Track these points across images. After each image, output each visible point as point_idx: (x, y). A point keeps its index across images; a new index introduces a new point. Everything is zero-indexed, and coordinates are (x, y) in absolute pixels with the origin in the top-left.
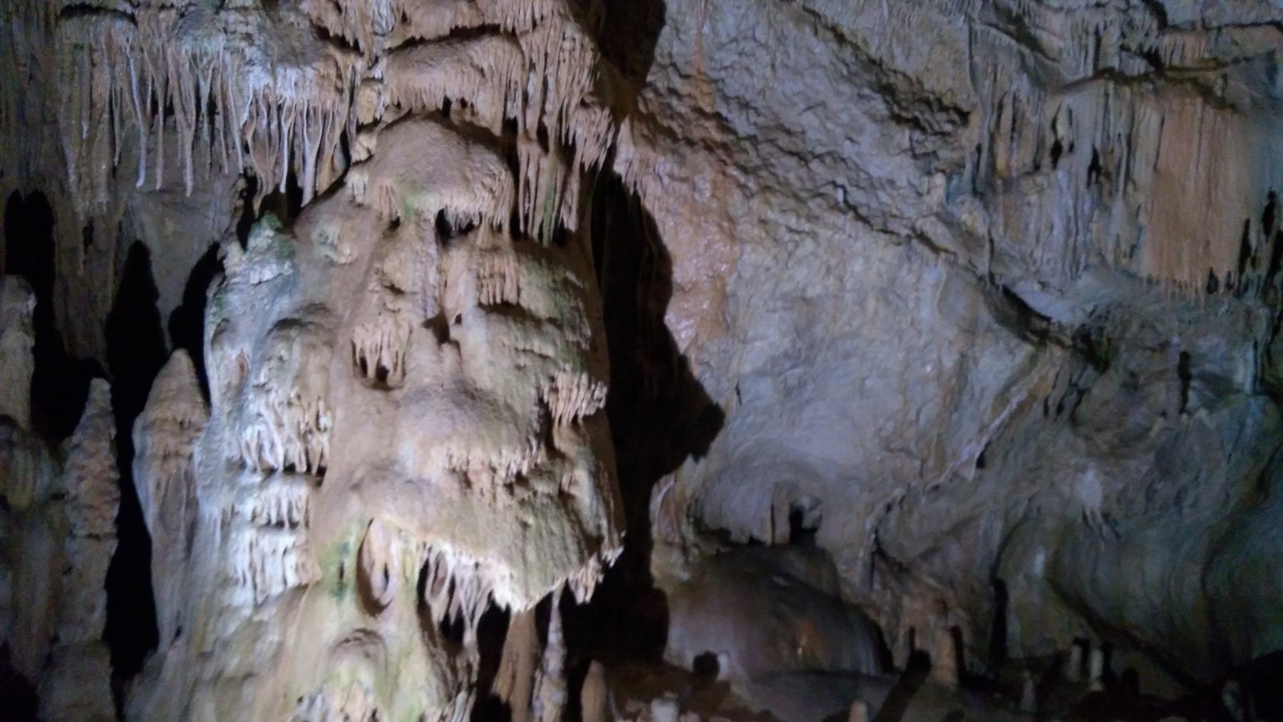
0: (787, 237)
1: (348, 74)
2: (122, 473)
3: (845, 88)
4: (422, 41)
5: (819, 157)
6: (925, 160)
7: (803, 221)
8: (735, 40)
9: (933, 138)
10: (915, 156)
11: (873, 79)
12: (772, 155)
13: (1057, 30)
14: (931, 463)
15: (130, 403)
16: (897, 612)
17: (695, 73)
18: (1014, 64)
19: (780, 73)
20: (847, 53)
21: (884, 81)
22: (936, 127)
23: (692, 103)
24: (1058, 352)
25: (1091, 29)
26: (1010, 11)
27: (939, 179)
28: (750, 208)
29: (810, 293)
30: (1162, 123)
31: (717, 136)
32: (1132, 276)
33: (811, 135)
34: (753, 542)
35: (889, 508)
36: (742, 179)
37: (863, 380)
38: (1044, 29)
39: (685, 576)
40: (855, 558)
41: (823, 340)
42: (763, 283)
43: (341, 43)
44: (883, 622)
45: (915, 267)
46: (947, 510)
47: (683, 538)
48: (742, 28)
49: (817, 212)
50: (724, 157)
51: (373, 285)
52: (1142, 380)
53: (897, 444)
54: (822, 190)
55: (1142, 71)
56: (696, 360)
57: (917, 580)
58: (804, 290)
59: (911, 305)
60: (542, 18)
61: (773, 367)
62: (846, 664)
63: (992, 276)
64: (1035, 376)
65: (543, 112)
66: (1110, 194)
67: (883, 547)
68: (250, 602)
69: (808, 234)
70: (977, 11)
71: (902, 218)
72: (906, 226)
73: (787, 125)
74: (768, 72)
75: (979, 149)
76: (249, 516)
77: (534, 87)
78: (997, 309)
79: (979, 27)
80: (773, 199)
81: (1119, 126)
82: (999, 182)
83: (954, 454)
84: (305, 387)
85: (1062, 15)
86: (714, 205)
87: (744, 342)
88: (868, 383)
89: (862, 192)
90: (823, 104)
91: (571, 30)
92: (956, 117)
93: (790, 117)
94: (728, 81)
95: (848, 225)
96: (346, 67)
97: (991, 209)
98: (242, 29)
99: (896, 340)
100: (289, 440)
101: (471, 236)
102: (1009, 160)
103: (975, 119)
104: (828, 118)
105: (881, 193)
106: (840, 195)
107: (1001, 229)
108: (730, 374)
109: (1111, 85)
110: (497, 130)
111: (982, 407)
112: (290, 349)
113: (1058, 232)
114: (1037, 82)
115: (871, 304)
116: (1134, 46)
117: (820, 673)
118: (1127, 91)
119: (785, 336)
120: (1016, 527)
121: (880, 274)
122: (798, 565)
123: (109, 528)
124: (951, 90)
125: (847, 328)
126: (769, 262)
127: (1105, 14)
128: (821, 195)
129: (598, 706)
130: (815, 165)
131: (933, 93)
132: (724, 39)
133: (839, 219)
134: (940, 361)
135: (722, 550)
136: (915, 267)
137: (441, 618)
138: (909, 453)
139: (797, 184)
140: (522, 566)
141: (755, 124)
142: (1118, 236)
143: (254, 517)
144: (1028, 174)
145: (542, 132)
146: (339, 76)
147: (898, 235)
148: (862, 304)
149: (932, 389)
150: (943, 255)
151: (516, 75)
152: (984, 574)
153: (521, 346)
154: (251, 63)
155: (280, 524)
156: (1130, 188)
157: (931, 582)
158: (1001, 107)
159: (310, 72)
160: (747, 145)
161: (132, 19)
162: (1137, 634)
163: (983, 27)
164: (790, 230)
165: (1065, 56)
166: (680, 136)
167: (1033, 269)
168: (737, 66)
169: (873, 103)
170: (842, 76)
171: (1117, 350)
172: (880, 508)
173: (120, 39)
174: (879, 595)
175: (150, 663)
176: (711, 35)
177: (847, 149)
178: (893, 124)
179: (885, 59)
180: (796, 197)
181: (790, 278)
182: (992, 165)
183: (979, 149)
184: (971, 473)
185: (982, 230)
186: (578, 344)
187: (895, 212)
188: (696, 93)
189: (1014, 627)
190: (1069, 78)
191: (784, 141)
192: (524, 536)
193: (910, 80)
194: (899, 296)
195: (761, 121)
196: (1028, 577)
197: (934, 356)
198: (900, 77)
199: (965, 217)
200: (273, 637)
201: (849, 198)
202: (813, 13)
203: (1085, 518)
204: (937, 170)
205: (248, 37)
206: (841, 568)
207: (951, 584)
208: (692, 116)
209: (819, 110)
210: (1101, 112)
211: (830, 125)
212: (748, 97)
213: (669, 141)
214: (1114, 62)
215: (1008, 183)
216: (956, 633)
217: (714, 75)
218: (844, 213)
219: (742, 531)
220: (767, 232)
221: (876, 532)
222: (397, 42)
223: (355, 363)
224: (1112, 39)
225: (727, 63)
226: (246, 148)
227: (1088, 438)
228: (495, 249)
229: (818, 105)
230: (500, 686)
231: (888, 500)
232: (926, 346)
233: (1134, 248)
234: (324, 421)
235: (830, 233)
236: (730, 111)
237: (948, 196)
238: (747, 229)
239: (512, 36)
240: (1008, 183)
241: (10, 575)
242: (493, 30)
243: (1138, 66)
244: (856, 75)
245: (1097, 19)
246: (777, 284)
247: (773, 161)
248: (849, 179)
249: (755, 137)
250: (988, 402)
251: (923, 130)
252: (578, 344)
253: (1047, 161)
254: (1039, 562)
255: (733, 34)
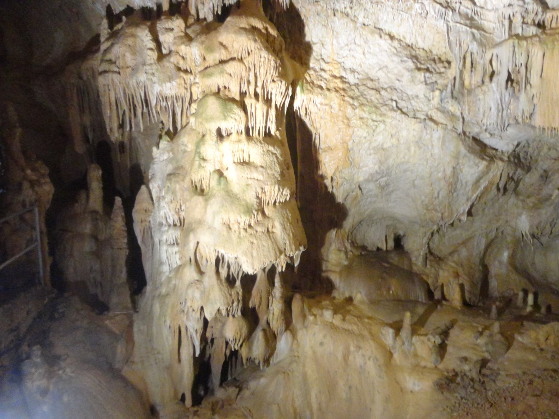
0: (372, 123)
1: (188, 82)
2: (128, 228)
3: (396, 59)
4: (210, 67)
5: (385, 89)
6: (431, 86)
7: (378, 116)
8: (347, 45)
9: (436, 75)
10: (426, 84)
11: (408, 53)
12: (364, 90)
13: (492, 20)
14: (446, 214)
15: (129, 205)
16: (437, 278)
17: (332, 61)
18: (470, 37)
19: (367, 56)
20: (396, 43)
21: (414, 53)
22: (437, 70)
23: (330, 73)
24: (500, 164)
25: (507, 17)
26: (467, 15)
27: (437, 93)
28: (355, 113)
29: (385, 146)
30: (544, 55)
31: (341, 86)
32: (534, 127)
33: (382, 80)
34: (378, 249)
35: (432, 234)
36: (351, 101)
37: (414, 181)
38: (485, 20)
39: (346, 263)
40: (420, 255)
41: (393, 165)
42: (364, 144)
43: (186, 71)
44: (430, 281)
45: (428, 132)
46: (459, 234)
47: (346, 248)
48: (349, 39)
49: (384, 112)
50: (343, 94)
51: (197, 158)
52: (550, 173)
53: (431, 207)
54: (387, 103)
55: (534, 33)
56: (340, 177)
57: (446, 264)
58: (382, 145)
59: (430, 148)
60: (251, 51)
61: (372, 178)
62: (412, 298)
63: (464, 133)
64: (491, 175)
65: (256, 86)
66: (519, 90)
67: (432, 251)
68: (168, 270)
69: (380, 121)
70: (450, 18)
71: (422, 111)
72: (424, 115)
73: (372, 78)
74: (362, 56)
75: (455, 78)
76: (165, 241)
77: (252, 79)
78: (469, 147)
79: (451, 24)
80: (365, 109)
81: (521, 60)
82: (466, 91)
83: (457, 210)
84: (176, 196)
85: (493, 13)
86: (341, 113)
87: (359, 168)
88: (416, 182)
89: (404, 102)
90: (386, 67)
91: (264, 53)
92: (446, 65)
93: (373, 74)
94: (346, 62)
95: (398, 116)
96: (187, 79)
97: (462, 103)
98: (150, 71)
99: (425, 163)
100: (173, 215)
101: (230, 136)
102: (471, 81)
103: (453, 65)
104: (388, 72)
105: (412, 102)
106: (394, 104)
107: (467, 112)
108: (355, 182)
109: (516, 41)
110: (238, 98)
111: (467, 189)
112: (171, 184)
113: (494, 110)
114: (481, 44)
115: (413, 149)
116: (530, 21)
117: (399, 301)
118: (524, 43)
119: (375, 165)
120: (492, 241)
121: (414, 136)
122: (395, 259)
123: (125, 246)
124: (445, 53)
125: (403, 160)
126: (365, 134)
127: (513, 8)
128: (386, 105)
129: (299, 309)
130: (383, 92)
131: (437, 55)
132: (342, 45)
133: (393, 114)
134: (444, 171)
135: (363, 253)
136: (428, 132)
137: (226, 276)
138: (436, 211)
139: (376, 101)
140: (251, 258)
141: (358, 78)
142: (523, 110)
143: (166, 241)
144: (479, 86)
145: (256, 95)
146: (185, 83)
147: (420, 119)
148: (409, 149)
149: (443, 183)
150: (440, 125)
151: (244, 74)
152: (477, 260)
153: (249, 177)
154: (154, 83)
155: (174, 244)
156: (528, 87)
157: (453, 264)
158: (464, 58)
159: (174, 83)
160: (354, 87)
161: (119, 73)
162: (554, 287)
163: (454, 24)
164: (373, 121)
165: (496, 30)
166: (324, 88)
167: (484, 128)
168: (349, 56)
169: (407, 63)
170: (394, 54)
171: (537, 161)
172: (429, 234)
173: (116, 80)
174: (429, 270)
175: (143, 291)
176: (337, 44)
177: (397, 85)
178: (417, 71)
179: (414, 44)
180: (376, 107)
181: (375, 140)
182: (462, 84)
183: (455, 78)
184: (464, 218)
185: (458, 113)
186: (273, 174)
187: (419, 109)
188: (332, 68)
189: (494, 284)
190: (498, 40)
191: (370, 84)
192: (252, 247)
193: (426, 51)
194: (424, 145)
195: (360, 77)
196: (500, 262)
197: (442, 169)
198: (421, 50)
199: (451, 108)
200: (173, 282)
201: (399, 105)
202: (379, 29)
203: (523, 236)
204: (437, 89)
205: (153, 74)
206: (413, 259)
207: (462, 266)
208: (331, 78)
209: (385, 69)
210: (511, 55)
211: (389, 75)
212: (355, 68)
213: (319, 90)
214: (519, 31)
215: (470, 92)
216: (462, 287)
217: (339, 60)
218: (396, 111)
219: (374, 245)
220: (363, 123)
221: (428, 244)
222: (202, 68)
223: (193, 186)
224: (518, 20)
225: (344, 55)
226: (158, 113)
227: (523, 201)
228: (239, 141)
229: (384, 67)
230: (254, 301)
231: (432, 231)
232: (438, 165)
233: (531, 115)
234: (183, 208)
235: (390, 120)
236: (346, 74)
237: (441, 100)
238: (355, 122)
239: (241, 60)
240: (470, 92)
241: (99, 262)
242: (233, 59)
243: (533, 30)
244: (400, 52)
245: (509, 11)
246: (370, 143)
247: (365, 93)
248: (398, 97)
249: (358, 84)
250: (469, 187)
251: (431, 72)
252: (273, 174)
253: (487, 79)
254: (506, 255)
255: (346, 42)
